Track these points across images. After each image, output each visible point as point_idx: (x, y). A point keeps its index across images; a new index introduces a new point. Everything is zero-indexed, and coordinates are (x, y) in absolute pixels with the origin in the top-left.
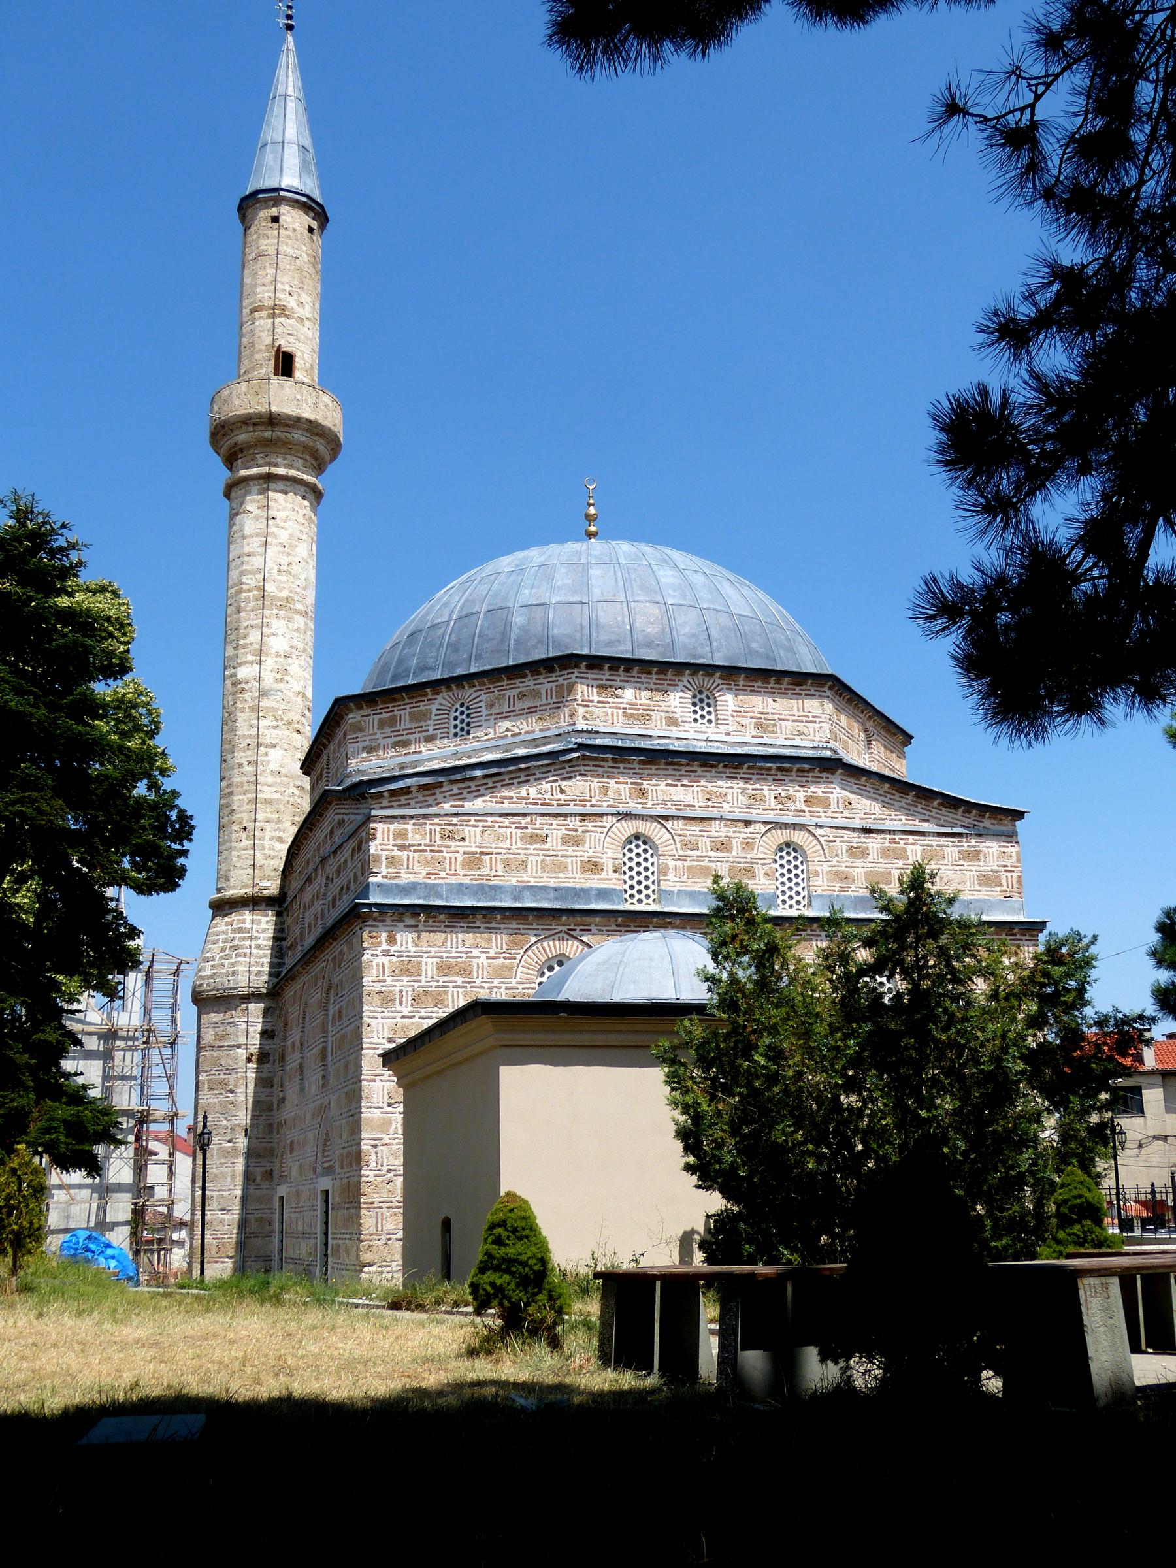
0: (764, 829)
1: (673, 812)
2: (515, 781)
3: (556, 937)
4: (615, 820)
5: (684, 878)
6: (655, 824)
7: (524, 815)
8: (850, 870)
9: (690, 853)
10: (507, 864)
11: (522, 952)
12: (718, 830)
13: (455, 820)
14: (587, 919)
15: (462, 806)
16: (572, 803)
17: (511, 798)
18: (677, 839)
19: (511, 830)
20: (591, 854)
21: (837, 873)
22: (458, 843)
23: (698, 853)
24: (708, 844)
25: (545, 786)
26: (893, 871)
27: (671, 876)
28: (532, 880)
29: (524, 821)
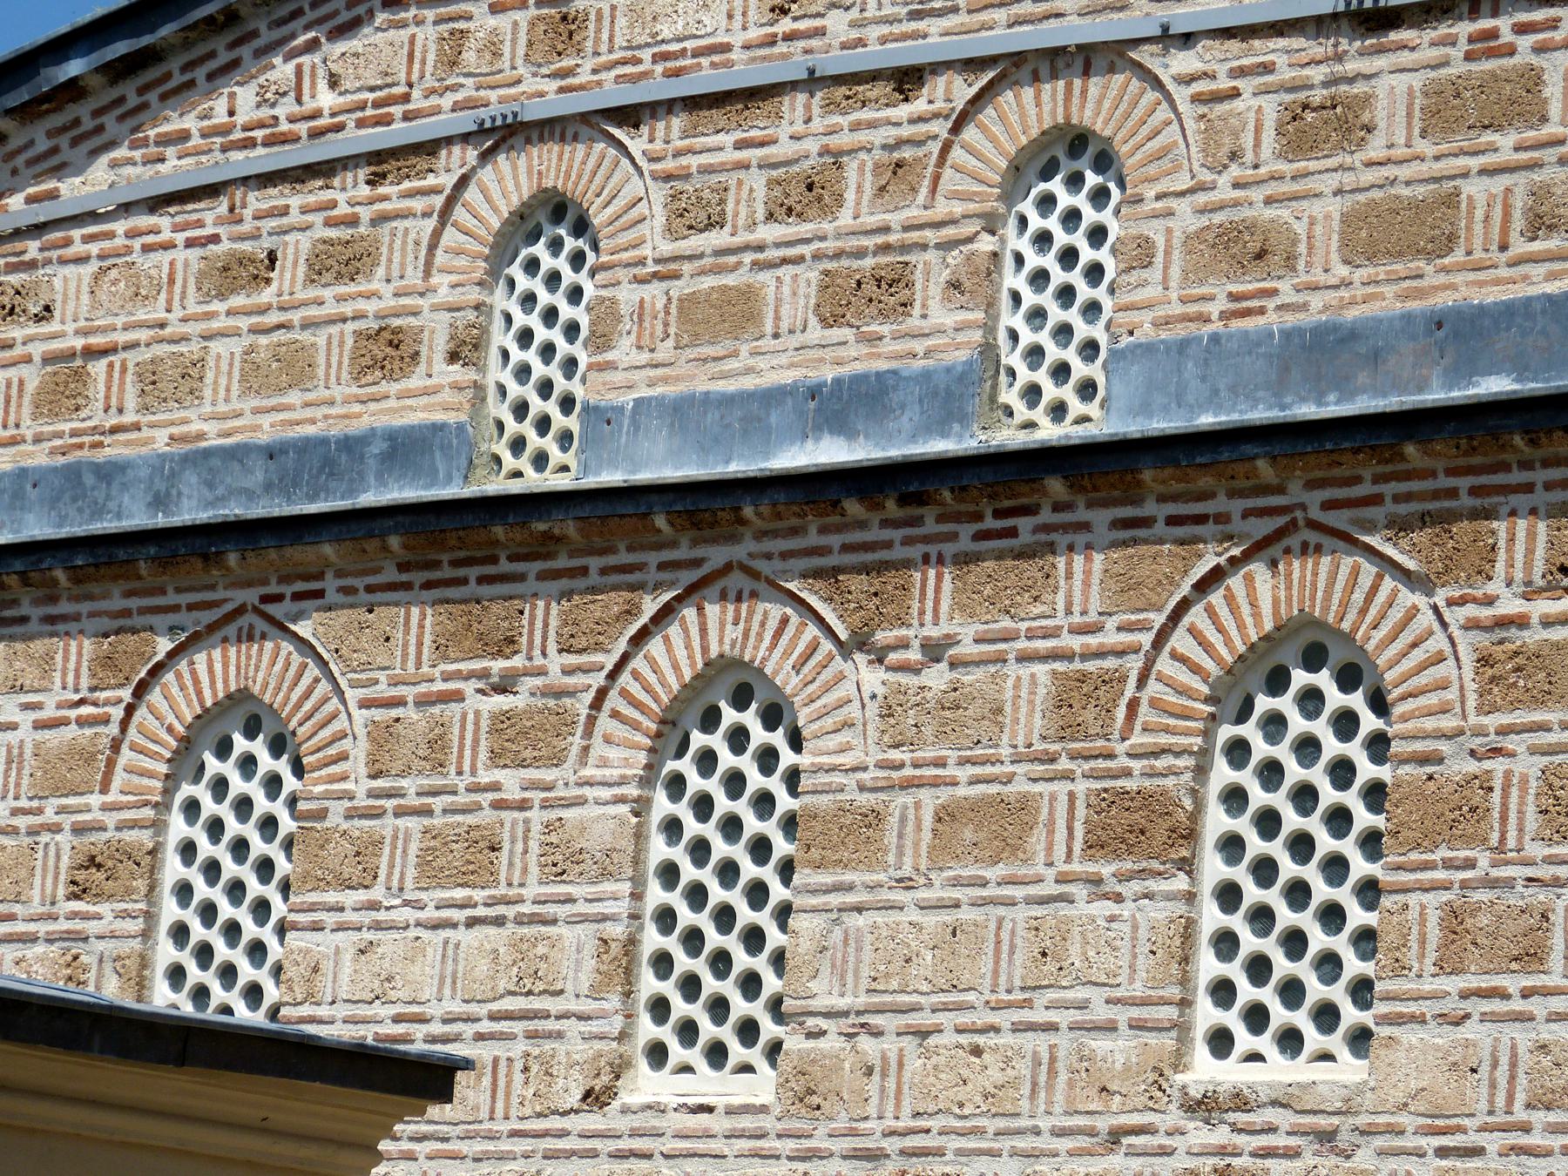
0: (962, 90)
1: (659, 88)
2: (200, 74)
3: (231, 630)
4: (472, 155)
5: (665, 351)
6: (600, 146)
7: (211, 191)
8: (1283, 213)
9: (697, 242)
10: (150, 378)
11: (126, 694)
12: (798, 130)
13: (32, 248)
14: (302, 554)
15: (53, 195)
16: (350, 120)
17: (184, 136)
18: (1181, 95)
19: (173, 252)
20: (389, 302)
21: (1227, 237)
22: (33, 329)
23: (717, 238)
24: (761, 193)
25: (282, 70)
26: (1474, 189)
27: (623, 351)
28: (211, 428)
29: (210, 214)
